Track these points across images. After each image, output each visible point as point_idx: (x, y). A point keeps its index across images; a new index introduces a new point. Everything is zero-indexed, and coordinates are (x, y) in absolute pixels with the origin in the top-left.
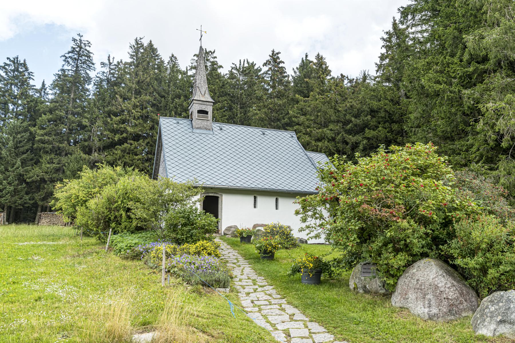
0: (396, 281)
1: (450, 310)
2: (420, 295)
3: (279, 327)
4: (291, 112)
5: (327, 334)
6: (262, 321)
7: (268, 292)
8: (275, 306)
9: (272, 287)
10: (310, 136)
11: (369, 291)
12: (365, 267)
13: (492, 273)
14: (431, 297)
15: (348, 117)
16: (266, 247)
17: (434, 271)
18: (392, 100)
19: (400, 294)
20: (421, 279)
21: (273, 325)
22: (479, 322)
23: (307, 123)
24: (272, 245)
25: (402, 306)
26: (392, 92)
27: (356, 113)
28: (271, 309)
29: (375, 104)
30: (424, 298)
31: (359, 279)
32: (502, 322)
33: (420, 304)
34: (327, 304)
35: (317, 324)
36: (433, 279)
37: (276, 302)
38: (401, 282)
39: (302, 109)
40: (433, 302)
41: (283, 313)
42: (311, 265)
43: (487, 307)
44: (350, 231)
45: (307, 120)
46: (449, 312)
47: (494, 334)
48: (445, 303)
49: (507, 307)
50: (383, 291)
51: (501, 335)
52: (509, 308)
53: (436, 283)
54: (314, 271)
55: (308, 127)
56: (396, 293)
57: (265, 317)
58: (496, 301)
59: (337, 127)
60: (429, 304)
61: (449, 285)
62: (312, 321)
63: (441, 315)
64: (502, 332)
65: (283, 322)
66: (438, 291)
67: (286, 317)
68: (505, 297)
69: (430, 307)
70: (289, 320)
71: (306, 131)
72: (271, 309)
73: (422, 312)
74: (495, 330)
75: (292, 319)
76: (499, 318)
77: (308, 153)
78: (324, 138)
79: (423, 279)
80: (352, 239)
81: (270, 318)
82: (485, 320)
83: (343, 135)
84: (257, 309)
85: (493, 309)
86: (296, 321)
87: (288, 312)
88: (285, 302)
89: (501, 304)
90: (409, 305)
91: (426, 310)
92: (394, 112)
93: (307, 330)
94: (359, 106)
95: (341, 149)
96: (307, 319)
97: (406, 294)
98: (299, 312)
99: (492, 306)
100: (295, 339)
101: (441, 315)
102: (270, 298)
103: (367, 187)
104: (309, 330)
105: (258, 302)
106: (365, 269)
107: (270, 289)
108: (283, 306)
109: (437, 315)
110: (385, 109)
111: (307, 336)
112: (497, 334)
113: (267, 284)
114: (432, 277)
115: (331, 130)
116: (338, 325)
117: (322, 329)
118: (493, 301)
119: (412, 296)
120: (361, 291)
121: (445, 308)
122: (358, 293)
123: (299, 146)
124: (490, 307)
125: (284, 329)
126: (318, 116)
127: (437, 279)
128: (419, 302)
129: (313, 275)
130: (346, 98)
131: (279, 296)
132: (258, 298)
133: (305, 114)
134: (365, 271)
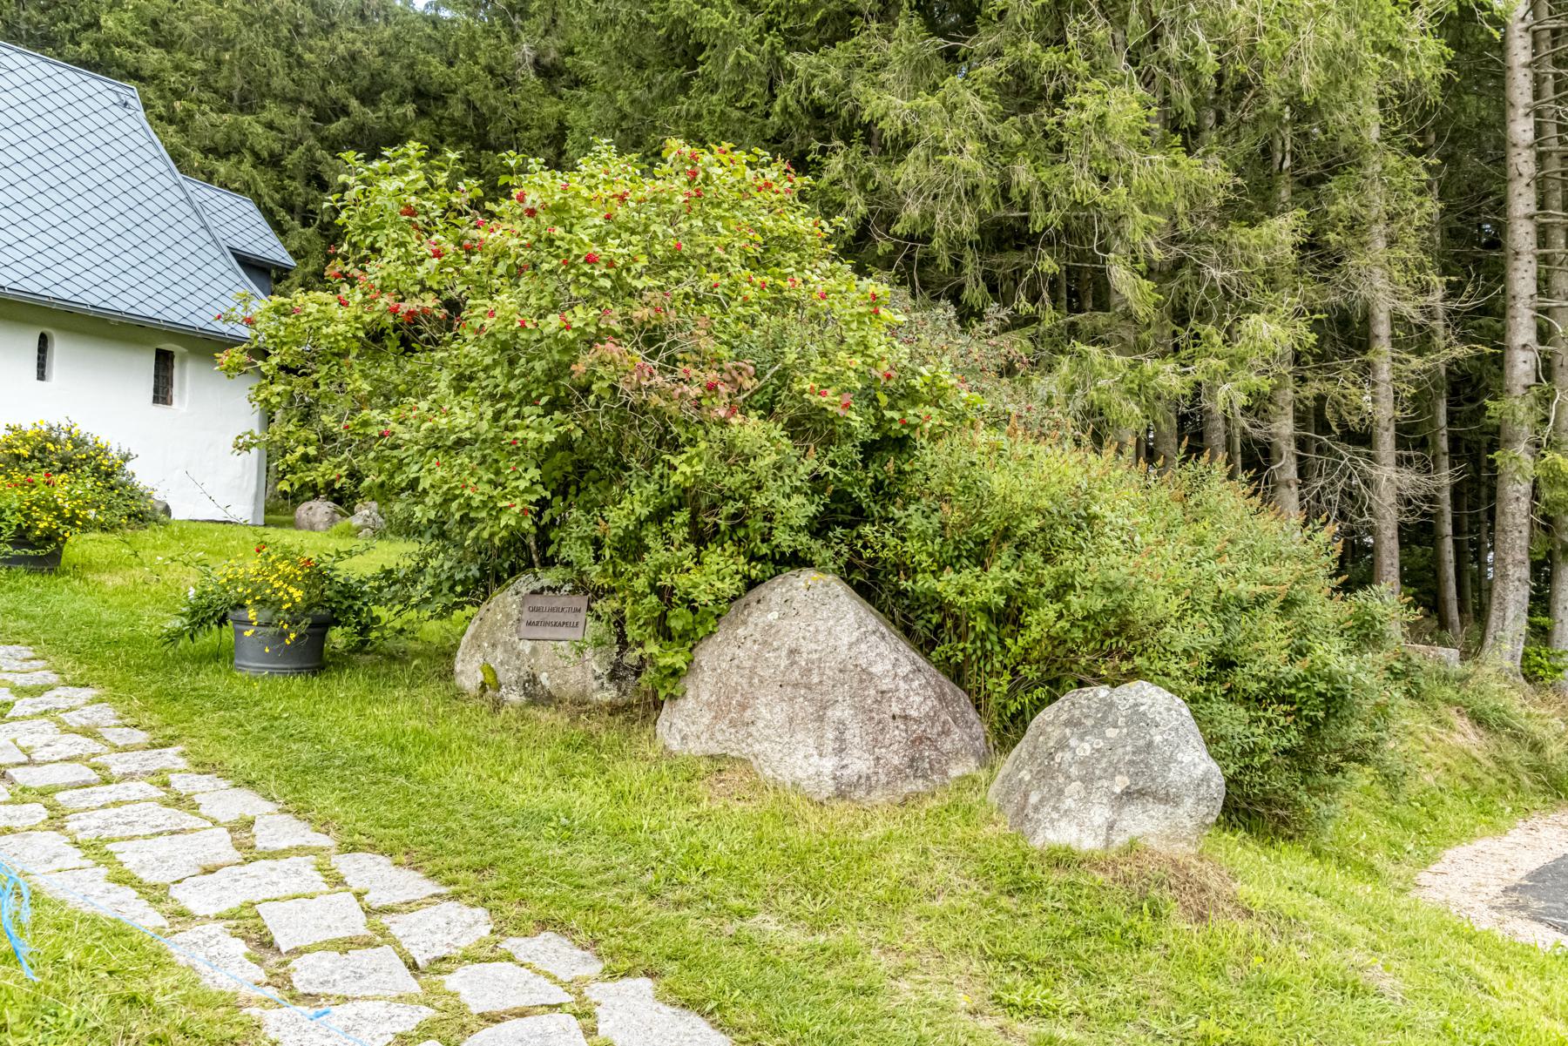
0: (689, 656)
1: (913, 760)
2: (806, 709)
3: (192, 898)
4: (108, 22)
5: (451, 908)
6: (85, 875)
7: (73, 719)
8: (135, 789)
9: (87, 693)
10: (184, 130)
11: (550, 697)
12: (538, 601)
13: (1042, 620)
14: (848, 713)
15: (334, 90)
16: (27, 516)
17: (851, 617)
18: (490, 70)
19: (709, 704)
20: (806, 647)
21: (155, 894)
22: (1034, 798)
23: (173, 79)
24: (58, 509)
25: (717, 751)
26: (493, 42)
27: (366, 83)
28: (117, 804)
29: (436, 68)
30: (821, 719)
31: (511, 649)
32: (1129, 795)
33: (805, 741)
34: (394, 761)
35: (385, 861)
36: (851, 646)
37: (134, 768)
38: (707, 655)
39: (155, 23)
40: (854, 733)
41: (190, 821)
42: (298, 595)
43: (1062, 745)
44: (516, 449)
45: (177, 68)
46: (911, 766)
47: (1108, 842)
48: (896, 733)
49: (1141, 743)
50: (609, 695)
51: (1132, 843)
52: (1150, 744)
53: (863, 662)
54: (306, 622)
55: (178, 95)
56: (688, 704)
57: (96, 850)
58: (1089, 722)
59: (295, 122)
60: (840, 739)
61: (906, 668)
62: (353, 848)
63: (883, 779)
64: (1136, 831)
65: (208, 871)
66: (872, 692)
67: (219, 845)
68: (1123, 708)
69: (842, 750)
70: (237, 856)
71: (170, 108)
72: (117, 804)
73: (812, 771)
74: (1111, 827)
75: (249, 853)
76: (1121, 783)
77: (189, 186)
78: (238, 151)
79: (813, 646)
80: (523, 484)
81: (131, 857)
82: (1061, 792)
83: (309, 149)
84: (37, 811)
85: (1085, 749)
86: (274, 855)
87: (218, 812)
88: (182, 763)
89: (1111, 733)
90: (757, 747)
91: (829, 764)
92: (494, 110)
93: (345, 899)
94: (378, 63)
95: (299, 201)
96: (322, 840)
97: (743, 707)
98: (269, 807)
99: (1082, 739)
100: (308, 959)
101: (883, 779)
102: (96, 747)
103: (612, 272)
104: (359, 896)
105: (33, 770)
106: (538, 610)
107: (80, 704)
108: (179, 783)
109: (868, 778)
110: (468, 94)
111: (362, 930)
112: (1120, 840)
113: (53, 678)
114: (846, 640)
115: (270, 126)
116: (488, 858)
117: (415, 885)
118: (1078, 724)
119: (769, 711)
120: (515, 697)
121: (896, 752)
122: (497, 705)
123: (150, 147)
124: (1073, 742)
125: (223, 908)
126: (219, 63)
127: (863, 647)
128: (800, 736)
129: (300, 637)
130: (333, 25)
131: (141, 737)
132: (26, 751)
133: (167, 45)
134: (535, 617)
